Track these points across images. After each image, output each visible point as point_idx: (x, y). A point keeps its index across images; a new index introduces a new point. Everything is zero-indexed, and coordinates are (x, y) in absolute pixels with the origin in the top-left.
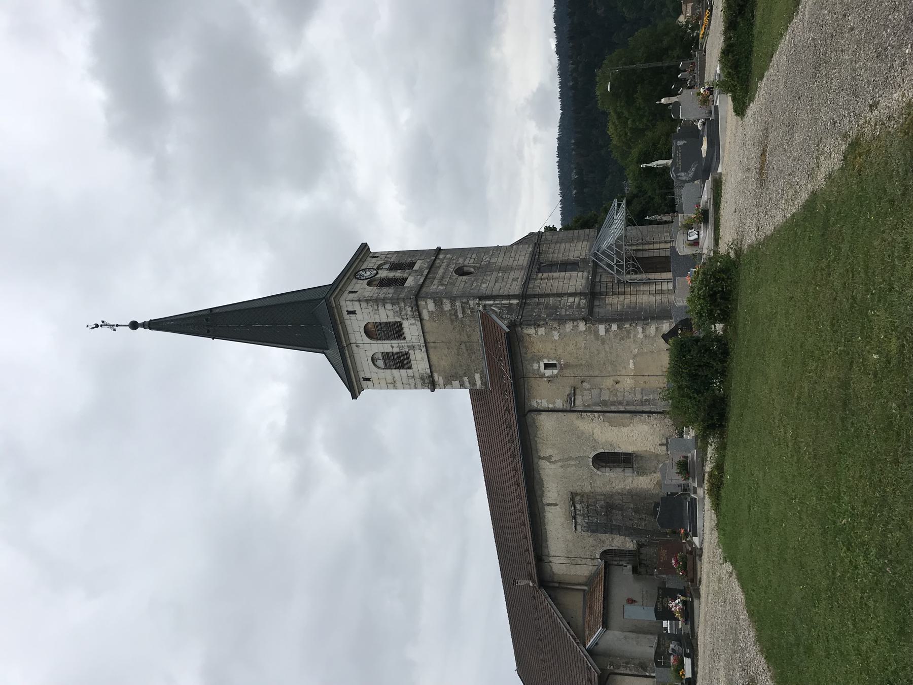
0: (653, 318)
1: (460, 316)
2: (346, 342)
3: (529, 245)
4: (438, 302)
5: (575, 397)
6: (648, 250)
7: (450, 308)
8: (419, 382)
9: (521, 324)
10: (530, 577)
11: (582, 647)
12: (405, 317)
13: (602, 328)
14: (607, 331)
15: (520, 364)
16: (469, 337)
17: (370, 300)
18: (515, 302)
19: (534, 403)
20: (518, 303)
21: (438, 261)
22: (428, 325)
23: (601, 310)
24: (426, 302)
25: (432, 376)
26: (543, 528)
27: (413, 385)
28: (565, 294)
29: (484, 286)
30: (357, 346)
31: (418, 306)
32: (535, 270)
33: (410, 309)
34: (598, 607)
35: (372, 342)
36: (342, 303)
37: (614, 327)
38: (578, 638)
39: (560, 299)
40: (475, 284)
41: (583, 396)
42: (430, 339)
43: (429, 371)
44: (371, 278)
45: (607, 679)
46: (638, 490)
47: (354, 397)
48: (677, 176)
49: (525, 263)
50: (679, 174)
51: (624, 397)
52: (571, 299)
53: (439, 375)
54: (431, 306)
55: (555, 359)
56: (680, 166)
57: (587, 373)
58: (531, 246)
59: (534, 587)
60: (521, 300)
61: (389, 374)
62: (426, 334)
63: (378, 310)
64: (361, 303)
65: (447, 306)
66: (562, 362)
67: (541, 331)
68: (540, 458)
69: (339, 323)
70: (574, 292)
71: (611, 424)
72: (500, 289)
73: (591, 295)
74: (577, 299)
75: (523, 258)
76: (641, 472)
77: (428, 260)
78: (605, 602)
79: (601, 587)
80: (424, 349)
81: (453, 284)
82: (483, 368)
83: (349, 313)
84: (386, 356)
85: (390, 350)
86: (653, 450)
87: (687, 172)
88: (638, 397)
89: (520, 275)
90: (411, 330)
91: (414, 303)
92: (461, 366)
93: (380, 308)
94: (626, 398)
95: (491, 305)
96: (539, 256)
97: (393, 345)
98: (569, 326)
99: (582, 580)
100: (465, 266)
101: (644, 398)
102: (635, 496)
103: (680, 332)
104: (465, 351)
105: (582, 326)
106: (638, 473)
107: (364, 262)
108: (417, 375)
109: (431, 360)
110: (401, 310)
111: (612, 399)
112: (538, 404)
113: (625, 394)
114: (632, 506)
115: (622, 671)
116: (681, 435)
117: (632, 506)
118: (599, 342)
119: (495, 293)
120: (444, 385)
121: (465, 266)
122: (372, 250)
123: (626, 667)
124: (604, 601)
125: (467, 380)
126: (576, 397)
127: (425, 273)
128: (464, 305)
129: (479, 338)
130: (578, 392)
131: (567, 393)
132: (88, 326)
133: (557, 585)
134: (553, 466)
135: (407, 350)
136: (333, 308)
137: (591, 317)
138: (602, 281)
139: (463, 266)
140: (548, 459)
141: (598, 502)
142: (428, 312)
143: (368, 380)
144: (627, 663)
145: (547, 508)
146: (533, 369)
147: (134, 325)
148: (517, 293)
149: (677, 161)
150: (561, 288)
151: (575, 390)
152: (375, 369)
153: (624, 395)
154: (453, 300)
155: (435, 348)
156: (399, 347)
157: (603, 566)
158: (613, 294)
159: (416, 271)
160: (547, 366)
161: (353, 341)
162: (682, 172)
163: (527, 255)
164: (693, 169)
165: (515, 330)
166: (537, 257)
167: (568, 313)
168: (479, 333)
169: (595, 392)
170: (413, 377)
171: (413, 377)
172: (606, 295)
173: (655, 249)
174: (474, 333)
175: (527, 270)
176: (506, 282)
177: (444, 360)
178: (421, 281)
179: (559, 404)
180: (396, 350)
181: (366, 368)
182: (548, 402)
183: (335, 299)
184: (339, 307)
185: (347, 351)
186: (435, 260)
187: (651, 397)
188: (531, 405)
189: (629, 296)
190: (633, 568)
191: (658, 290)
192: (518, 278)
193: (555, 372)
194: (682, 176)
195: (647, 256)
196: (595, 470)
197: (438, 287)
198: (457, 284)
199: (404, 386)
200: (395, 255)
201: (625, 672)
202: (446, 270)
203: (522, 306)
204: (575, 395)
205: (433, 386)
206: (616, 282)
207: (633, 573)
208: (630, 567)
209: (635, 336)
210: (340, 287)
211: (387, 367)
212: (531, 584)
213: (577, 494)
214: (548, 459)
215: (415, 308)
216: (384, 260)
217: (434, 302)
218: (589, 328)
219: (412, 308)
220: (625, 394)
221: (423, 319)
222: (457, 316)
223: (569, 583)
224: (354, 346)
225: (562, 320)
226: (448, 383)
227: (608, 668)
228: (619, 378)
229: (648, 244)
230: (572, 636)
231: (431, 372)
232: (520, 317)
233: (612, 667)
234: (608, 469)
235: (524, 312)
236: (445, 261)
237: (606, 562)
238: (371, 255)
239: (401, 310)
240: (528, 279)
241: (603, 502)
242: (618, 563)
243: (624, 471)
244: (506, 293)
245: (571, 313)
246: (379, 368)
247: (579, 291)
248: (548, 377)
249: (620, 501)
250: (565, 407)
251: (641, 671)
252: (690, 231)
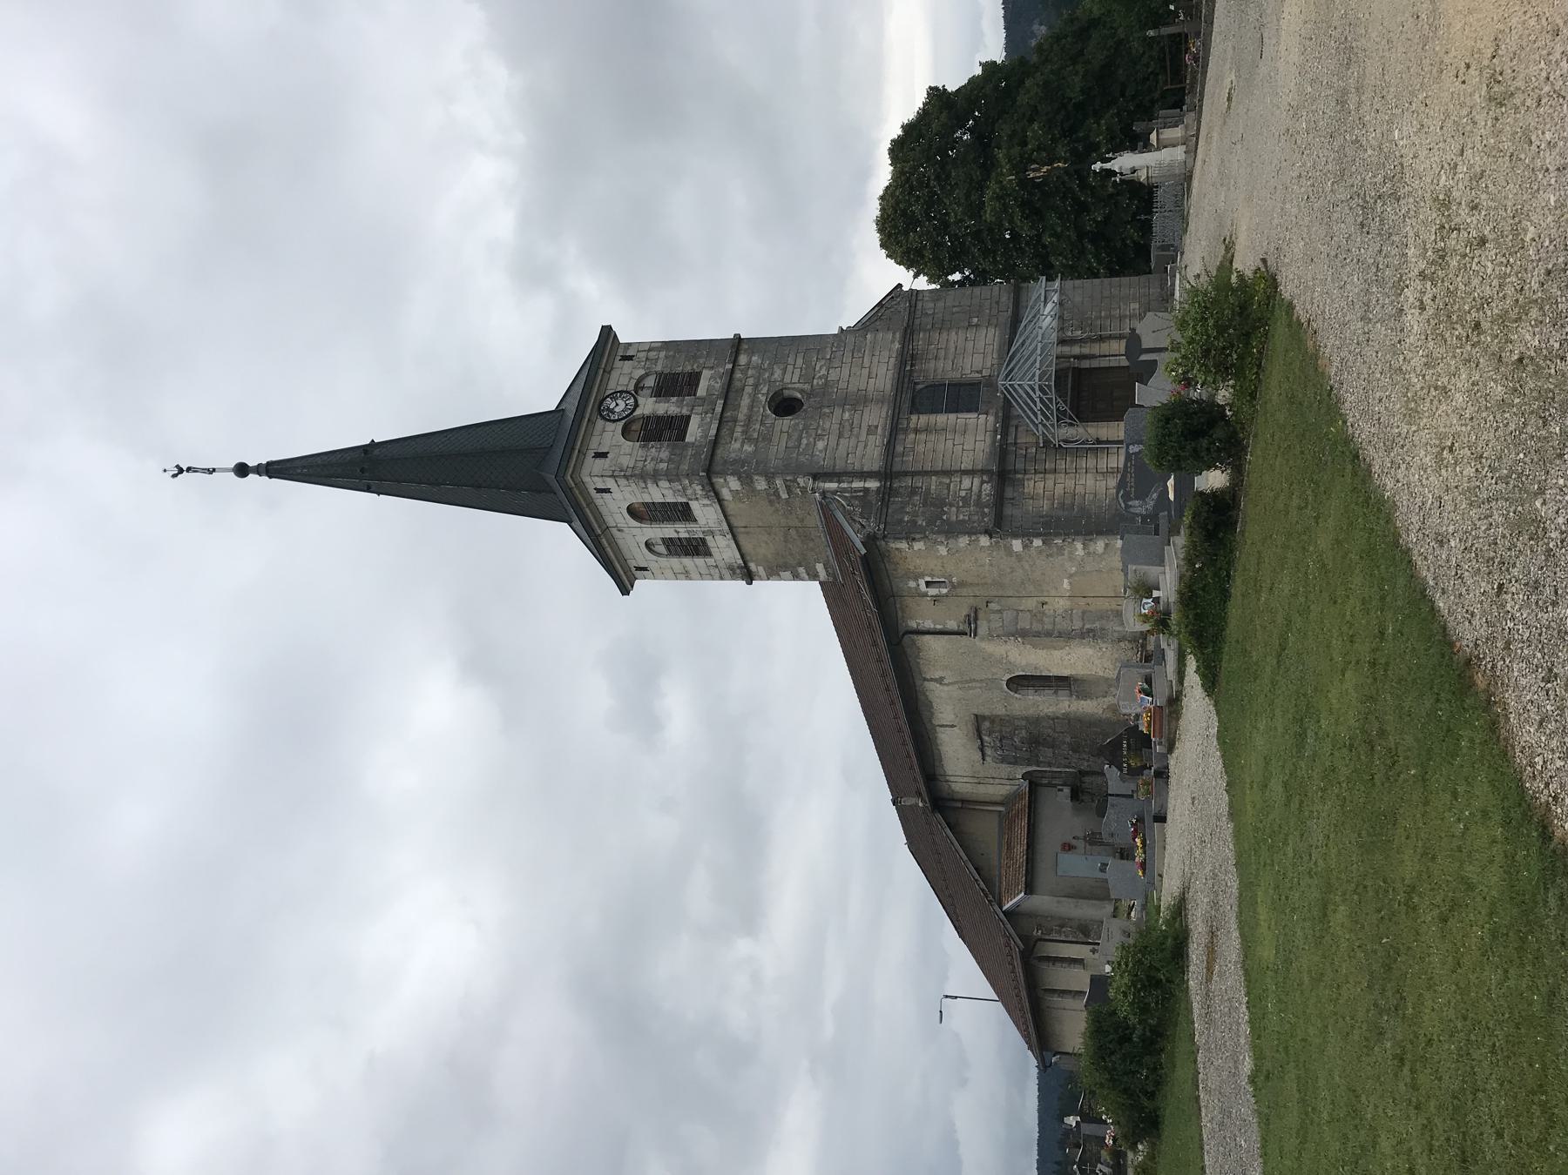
0: (1100, 533)
1: (784, 496)
2: (600, 527)
3: (894, 333)
4: (746, 480)
5: (976, 623)
6: (1100, 356)
7: (767, 487)
8: (726, 573)
9: (885, 537)
10: (919, 794)
11: (996, 907)
12: (694, 497)
13: (1017, 545)
14: (1025, 547)
15: (887, 581)
16: (802, 521)
17: (631, 476)
18: (873, 484)
19: (913, 624)
20: (879, 488)
21: (738, 375)
22: (731, 507)
23: (1016, 512)
24: (725, 480)
25: (746, 566)
26: (934, 747)
27: (718, 575)
28: (957, 471)
29: (821, 445)
30: (619, 530)
31: (712, 485)
32: (906, 406)
33: (700, 487)
34: (1020, 849)
35: (643, 525)
36: (587, 479)
37: (1037, 542)
38: (991, 893)
39: (948, 481)
40: (804, 441)
41: (989, 621)
42: (735, 522)
43: (740, 562)
44: (627, 416)
45: (1035, 945)
46: (1078, 714)
47: (625, 591)
48: (1127, 507)
49: (889, 386)
50: (1130, 503)
51: (1054, 625)
52: (966, 483)
53: (757, 565)
54: (734, 483)
55: (943, 576)
56: (1133, 489)
57: (995, 593)
58: (898, 335)
59: (924, 808)
60: (883, 483)
61: (675, 562)
62: (729, 518)
63: (647, 488)
64: (617, 479)
65: (761, 484)
66: (954, 580)
67: (918, 546)
68: (925, 679)
69: (585, 506)
70: (971, 468)
71: (1035, 646)
72: (848, 454)
73: (999, 476)
74: (977, 481)
75: (880, 374)
76: (1084, 695)
77: (721, 370)
78: (1029, 876)
79: (1024, 822)
80: (729, 536)
81: (767, 439)
82: (828, 557)
83: (599, 491)
84: (668, 542)
85: (675, 535)
86: (1101, 674)
87: (1144, 500)
88: (1077, 625)
89: (877, 416)
90: (706, 514)
91: (706, 481)
92: (791, 554)
93: (649, 485)
94: (1058, 627)
95: (834, 492)
96: (911, 367)
97: (678, 530)
98: (963, 541)
99: (999, 799)
100: (786, 389)
101: (1087, 626)
102: (1074, 723)
103: (1125, 746)
104: (796, 537)
105: (984, 541)
106: (1078, 697)
107: (610, 371)
108: (721, 564)
109: (742, 548)
110: (684, 489)
111: (1037, 627)
112: (918, 624)
113: (1057, 619)
114: (1068, 739)
115: (1054, 936)
116: (1108, 963)
117: (1068, 739)
118: (1013, 559)
119: (840, 466)
120: (767, 576)
121: (786, 389)
122: (623, 339)
123: (1059, 932)
124: (1027, 850)
125: (804, 571)
126: (978, 622)
127: (719, 409)
128: (788, 483)
129: (819, 524)
130: (981, 614)
131: (965, 613)
132: (165, 471)
133: (959, 805)
134: (946, 688)
135: (702, 536)
136: (571, 489)
137: (999, 525)
138: (1018, 441)
139: (782, 390)
140: (940, 681)
141: (1017, 732)
142: (730, 491)
143: (645, 569)
144: (1062, 926)
145: (938, 729)
146: (909, 587)
147: (242, 470)
148: (875, 467)
149: (1128, 480)
150: (949, 463)
151: (976, 612)
152: (655, 558)
153: (1054, 621)
154: (770, 478)
155: (747, 533)
156: (688, 532)
157: (1027, 789)
158: (1036, 472)
159: (703, 399)
160: (928, 584)
161: (611, 523)
162: (1136, 499)
163: (892, 360)
164: (1155, 496)
165: (876, 545)
166: (908, 368)
167: (961, 517)
168: (818, 517)
169: (1008, 616)
170: (717, 566)
171: (717, 566)
172: (1025, 473)
173: (1112, 356)
174: (808, 516)
175: (892, 405)
176: (858, 436)
177: (760, 547)
178: (713, 432)
179: (952, 625)
180: (683, 535)
181: (634, 537)
182: (935, 623)
183: (574, 476)
184: (581, 486)
185: (604, 540)
186: (733, 371)
187: (1097, 625)
188: (907, 625)
189: (1063, 476)
190: (1072, 791)
191: (1111, 468)
192: (877, 427)
193: (944, 591)
194: (1134, 507)
195: (1098, 366)
196: (1012, 693)
197: (742, 446)
198: (775, 439)
199: (702, 577)
200: (663, 354)
201: (1058, 938)
202: (754, 400)
203: (886, 494)
204: (976, 619)
205: (749, 577)
206: (1042, 445)
207: (1071, 800)
208: (1067, 790)
209: (1071, 553)
210: (578, 447)
211: (671, 553)
212: (921, 804)
213: (984, 718)
214: (940, 681)
215: (708, 488)
216: (644, 368)
217: (739, 479)
218: (997, 543)
219: (703, 486)
220: (1057, 619)
221: (723, 500)
222: (779, 497)
223: (976, 802)
224: (614, 531)
225: (952, 531)
226: (773, 573)
227: (1034, 933)
228: (1046, 599)
229: (1101, 339)
230: (983, 890)
231: (744, 562)
232: (882, 526)
233: (1040, 932)
234: (1031, 691)
235: (890, 511)
236: (750, 372)
237: (1030, 783)
238: (620, 353)
239: (684, 489)
240: (895, 430)
241: (1024, 732)
242: (1049, 783)
243: (1056, 693)
244: (857, 467)
245: (967, 518)
246: (659, 554)
247: (980, 467)
248: (932, 596)
249: (1050, 730)
250: (961, 628)
251: (1081, 937)
252: (1145, 601)
